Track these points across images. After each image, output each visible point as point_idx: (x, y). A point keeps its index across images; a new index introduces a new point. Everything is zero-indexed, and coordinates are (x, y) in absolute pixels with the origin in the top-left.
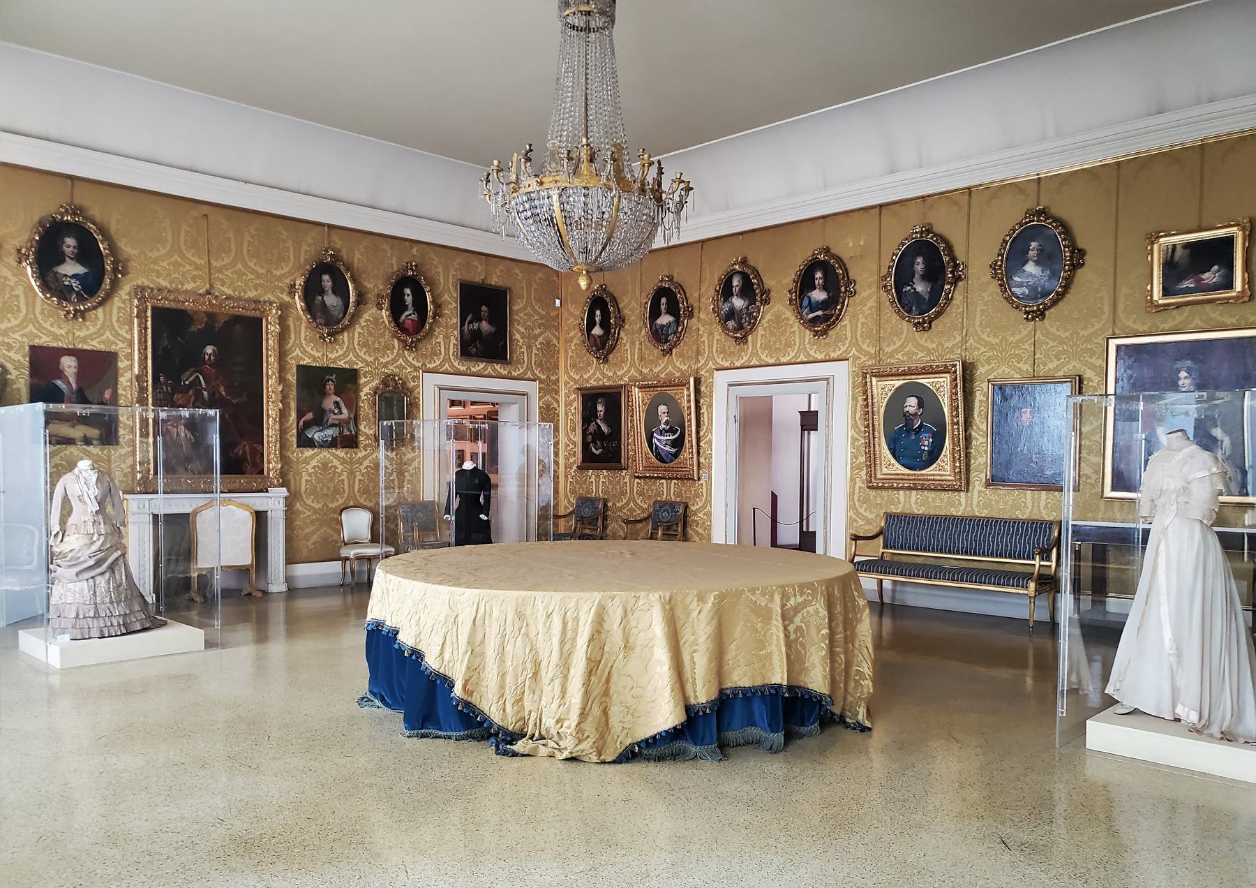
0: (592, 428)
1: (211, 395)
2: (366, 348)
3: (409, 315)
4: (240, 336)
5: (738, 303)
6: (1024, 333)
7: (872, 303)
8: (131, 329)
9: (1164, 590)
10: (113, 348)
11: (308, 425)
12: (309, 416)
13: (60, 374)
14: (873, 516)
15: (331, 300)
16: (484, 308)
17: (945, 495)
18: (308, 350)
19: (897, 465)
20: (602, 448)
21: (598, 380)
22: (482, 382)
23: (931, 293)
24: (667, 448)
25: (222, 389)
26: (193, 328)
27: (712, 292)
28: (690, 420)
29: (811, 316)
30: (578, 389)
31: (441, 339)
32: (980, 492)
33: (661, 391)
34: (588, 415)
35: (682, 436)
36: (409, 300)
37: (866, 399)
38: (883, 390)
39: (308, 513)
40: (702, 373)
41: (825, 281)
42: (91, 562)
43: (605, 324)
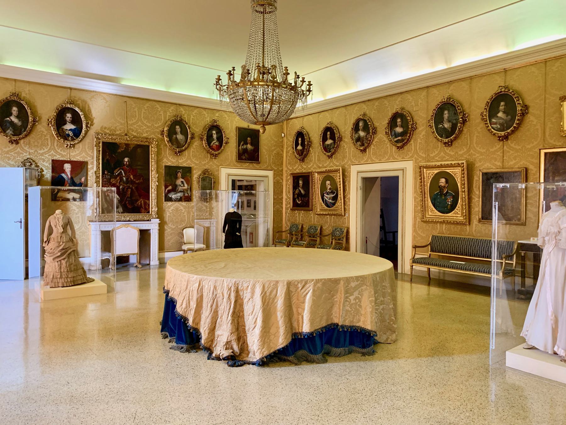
0: (297, 192)
1: (127, 179)
2: (194, 158)
3: (215, 143)
4: (139, 153)
5: (362, 134)
6: (498, 147)
7: (423, 133)
8: (93, 152)
9: (548, 285)
10: (86, 160)
11: (169, 191)
12: (170, 188)
13: (64, 171)
14: (425, 235)
15: (180, 137)
16: (249, 139)
17: (459, 227)
18: (170, 160)
19: (436, 211)
20: (302, 201)
21: (300, 169)
22: (246, 173)
23: (451, 128)
24: (330, 201)
25: (132, 176)
26: (119, 151)
27: (350, 129)
28: (340, 188)
29: (396, 139)
30: (291, 174)
31: (229, 153)
32: (476, 225)
33: (328, 176)
34: (295, 186)
35: (337, 195)
36: (215, 136)
37: (421, 179)
38: (429, 174)
39: (169, 230)
40: (346, 166)
41: (402, 123)
42: (59, 254)
43: (303, 144)
